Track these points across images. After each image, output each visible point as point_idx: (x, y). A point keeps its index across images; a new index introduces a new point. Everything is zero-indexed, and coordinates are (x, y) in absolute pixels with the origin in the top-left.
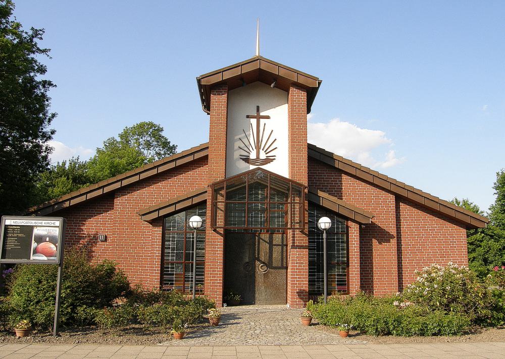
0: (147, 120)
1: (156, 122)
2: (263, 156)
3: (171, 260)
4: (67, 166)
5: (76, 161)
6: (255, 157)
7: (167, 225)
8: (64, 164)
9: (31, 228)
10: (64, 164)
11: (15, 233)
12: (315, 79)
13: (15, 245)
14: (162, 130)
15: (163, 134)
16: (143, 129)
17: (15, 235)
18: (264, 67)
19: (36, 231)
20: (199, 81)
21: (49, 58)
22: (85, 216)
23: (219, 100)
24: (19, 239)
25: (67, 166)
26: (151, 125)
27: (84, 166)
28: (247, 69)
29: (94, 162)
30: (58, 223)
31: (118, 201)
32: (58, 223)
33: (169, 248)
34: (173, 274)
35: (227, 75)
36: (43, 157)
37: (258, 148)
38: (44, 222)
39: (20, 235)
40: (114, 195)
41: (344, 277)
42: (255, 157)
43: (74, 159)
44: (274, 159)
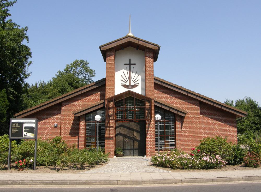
0: (79, 59)
1: (85, 59)
2: (132, 84)
3: (89, 135)
4: (38, 85)
5: (43, 83)
6: (129, 85)
7: (87, 118)
8: (36, 84)
9: (23, 123)
10: (36, 84)
11: (16, 126)
12: (157, 46)
13: (16, 131)
14: (88, 63)
15: (88, 65)
16: (76, 64)
17: (16, 127)
18: (132, 40)
19: (25, 125)
20: (100, 48)
21: (27, 42)
22: (47, 114)
23: (111, 59)
24: (18, 128)
25: (38, 85)
26: (81, 62)
27: (46, 86)
28: (123, 41)
29: (50, 84)
30: (34, 121)
31: (63, 108)
32: (34, 121)
33: (88, 130)
34: (90, 142)
35: (114, 45)
36: (22, 77)
37: (130, 80)
38: (28, 121)
39: (18, 127)
40: (61, 104)
41: (90, 143)
42: (129, 85)
43: (41, 81)
44: (138, 85)
